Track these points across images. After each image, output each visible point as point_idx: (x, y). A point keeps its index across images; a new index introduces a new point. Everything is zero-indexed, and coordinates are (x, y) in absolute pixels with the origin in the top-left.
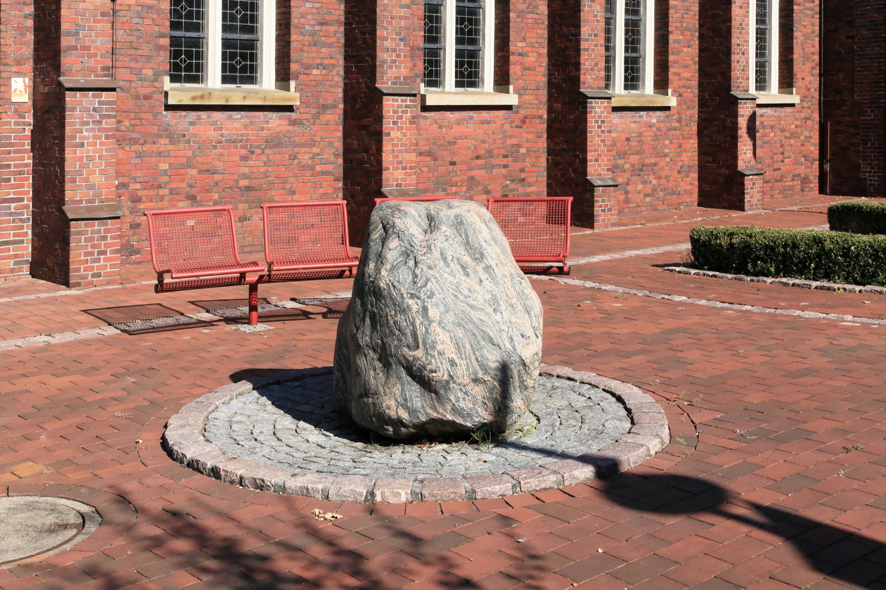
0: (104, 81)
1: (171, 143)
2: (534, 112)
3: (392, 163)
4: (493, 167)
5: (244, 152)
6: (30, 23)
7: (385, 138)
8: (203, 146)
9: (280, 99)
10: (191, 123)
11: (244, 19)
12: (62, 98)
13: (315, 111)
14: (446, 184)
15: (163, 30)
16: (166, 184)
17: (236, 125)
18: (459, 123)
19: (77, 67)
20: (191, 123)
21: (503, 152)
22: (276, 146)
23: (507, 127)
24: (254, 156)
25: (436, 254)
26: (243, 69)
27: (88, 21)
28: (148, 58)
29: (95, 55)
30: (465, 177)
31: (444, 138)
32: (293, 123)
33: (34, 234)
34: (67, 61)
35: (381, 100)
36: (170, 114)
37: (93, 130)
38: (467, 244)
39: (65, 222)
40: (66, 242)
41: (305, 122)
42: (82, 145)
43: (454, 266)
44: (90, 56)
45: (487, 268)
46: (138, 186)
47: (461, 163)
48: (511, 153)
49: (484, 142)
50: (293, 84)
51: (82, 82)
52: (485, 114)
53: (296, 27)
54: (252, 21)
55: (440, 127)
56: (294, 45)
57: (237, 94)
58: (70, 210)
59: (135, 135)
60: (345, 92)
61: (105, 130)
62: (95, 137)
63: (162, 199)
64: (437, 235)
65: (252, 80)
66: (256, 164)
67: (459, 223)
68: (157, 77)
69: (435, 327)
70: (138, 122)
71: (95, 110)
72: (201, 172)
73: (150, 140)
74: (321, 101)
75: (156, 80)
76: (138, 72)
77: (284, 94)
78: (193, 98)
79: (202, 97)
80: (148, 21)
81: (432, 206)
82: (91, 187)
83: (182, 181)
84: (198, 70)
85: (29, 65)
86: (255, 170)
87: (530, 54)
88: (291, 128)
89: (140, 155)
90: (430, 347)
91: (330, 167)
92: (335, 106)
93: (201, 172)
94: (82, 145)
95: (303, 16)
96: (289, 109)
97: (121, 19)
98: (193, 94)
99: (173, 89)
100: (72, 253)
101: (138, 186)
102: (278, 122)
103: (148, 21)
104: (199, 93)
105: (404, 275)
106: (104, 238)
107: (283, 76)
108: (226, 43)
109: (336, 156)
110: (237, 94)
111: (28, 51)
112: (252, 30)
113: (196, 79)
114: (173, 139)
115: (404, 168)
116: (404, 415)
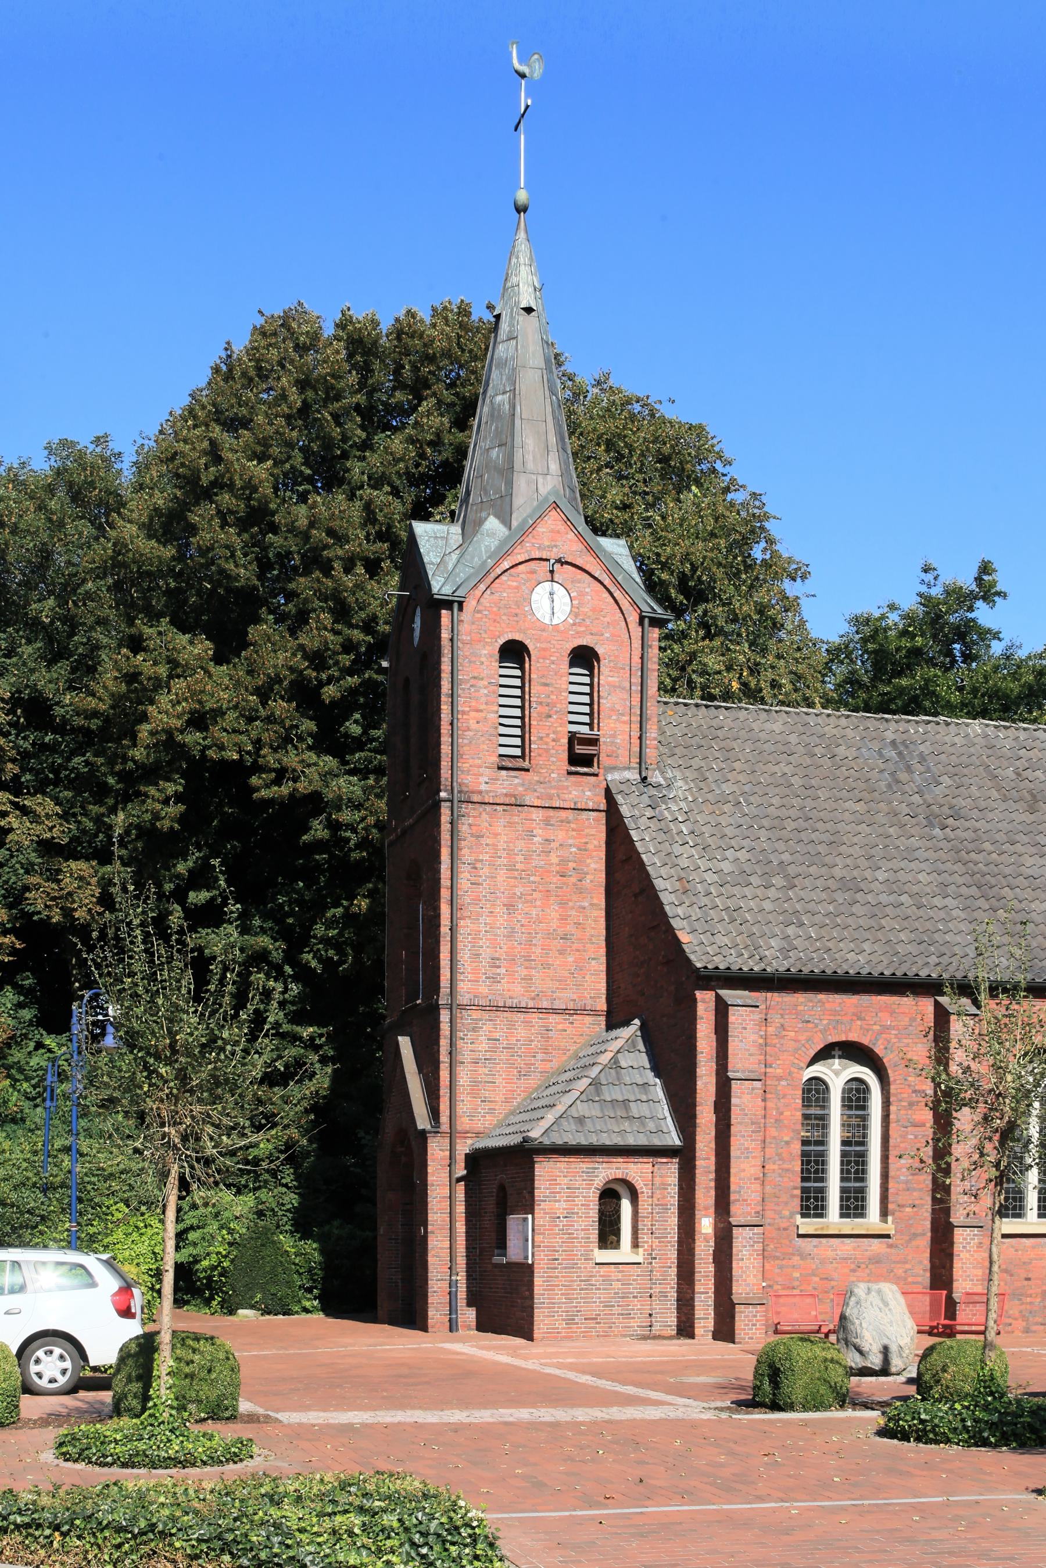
0: (755, 1220)
1: (802, 1259)
3: (961, 1276)
5: (853, 1266)
6: (712, 1184)
7: (955, 1258)
8: (823, 1262)
11: (857, 1172)
12: (731, 1232)
13: (908, 1238)
18: (1033, 1248)
19: (739, 1212)
20: (815, 1246)
22: (877, 1262)
25: (869, 1303)
26: (856, 1208)
28: (786, 1203)
30: (1040, 1290)
32: (890, 1246)
33: (715, 1314)
34: (734, 1209)
35: (953, 1231)
36: (801, 1239)
38: (882, 1300)
39: (733, 1305)
40: (733, 1317)
43: (876, 1308)
45: (890, 1310)
50: (890, 1218)
51: (742, 1221)
53: (893, 1178)
54: (863, 1173)
55: (1016, 1250)
56: (891, 1191)
57: (850, 1225)
58: (735, 1298)
59: (777, 1254)
60: (932, 1223)
64: (871, 1296)
65: (862, 1215)
67: (879, 1292)
68: (792, 1215)
69: (864, 1331)
72: (821, 1279)
74: (913, 1231)
76: (779, 1213)
77: (884, 1225)
78: (816, 1230)
79: (822, 1229)
80: (786, 1179)
81: (870, 1285)
82: (748, 1285)
85: (712, 1210)
88: (888, 1250)
89: (781, 1267)
90: (862, 1338)
91: (920, 1279)
92: (924, 1235)
93: (821, 1279)
95: (899, 1169)
96: (888, 1236)
97: (768, 1178)
99: (802, 1223)
100: (737, 1324)
101: (779, 1287)
103: (786, 1179)
105: (855, 1311)
106: (755, 1316)
107: (884, 1213)
108: (843, 1190)
109: (924, 1270)
110: (850, 1225)
111: (711, 1201)
112: (862, 1180)
113: (821, 1216)
114: (803, 1256)
115: (972, 1280)
116: (853, 1365)
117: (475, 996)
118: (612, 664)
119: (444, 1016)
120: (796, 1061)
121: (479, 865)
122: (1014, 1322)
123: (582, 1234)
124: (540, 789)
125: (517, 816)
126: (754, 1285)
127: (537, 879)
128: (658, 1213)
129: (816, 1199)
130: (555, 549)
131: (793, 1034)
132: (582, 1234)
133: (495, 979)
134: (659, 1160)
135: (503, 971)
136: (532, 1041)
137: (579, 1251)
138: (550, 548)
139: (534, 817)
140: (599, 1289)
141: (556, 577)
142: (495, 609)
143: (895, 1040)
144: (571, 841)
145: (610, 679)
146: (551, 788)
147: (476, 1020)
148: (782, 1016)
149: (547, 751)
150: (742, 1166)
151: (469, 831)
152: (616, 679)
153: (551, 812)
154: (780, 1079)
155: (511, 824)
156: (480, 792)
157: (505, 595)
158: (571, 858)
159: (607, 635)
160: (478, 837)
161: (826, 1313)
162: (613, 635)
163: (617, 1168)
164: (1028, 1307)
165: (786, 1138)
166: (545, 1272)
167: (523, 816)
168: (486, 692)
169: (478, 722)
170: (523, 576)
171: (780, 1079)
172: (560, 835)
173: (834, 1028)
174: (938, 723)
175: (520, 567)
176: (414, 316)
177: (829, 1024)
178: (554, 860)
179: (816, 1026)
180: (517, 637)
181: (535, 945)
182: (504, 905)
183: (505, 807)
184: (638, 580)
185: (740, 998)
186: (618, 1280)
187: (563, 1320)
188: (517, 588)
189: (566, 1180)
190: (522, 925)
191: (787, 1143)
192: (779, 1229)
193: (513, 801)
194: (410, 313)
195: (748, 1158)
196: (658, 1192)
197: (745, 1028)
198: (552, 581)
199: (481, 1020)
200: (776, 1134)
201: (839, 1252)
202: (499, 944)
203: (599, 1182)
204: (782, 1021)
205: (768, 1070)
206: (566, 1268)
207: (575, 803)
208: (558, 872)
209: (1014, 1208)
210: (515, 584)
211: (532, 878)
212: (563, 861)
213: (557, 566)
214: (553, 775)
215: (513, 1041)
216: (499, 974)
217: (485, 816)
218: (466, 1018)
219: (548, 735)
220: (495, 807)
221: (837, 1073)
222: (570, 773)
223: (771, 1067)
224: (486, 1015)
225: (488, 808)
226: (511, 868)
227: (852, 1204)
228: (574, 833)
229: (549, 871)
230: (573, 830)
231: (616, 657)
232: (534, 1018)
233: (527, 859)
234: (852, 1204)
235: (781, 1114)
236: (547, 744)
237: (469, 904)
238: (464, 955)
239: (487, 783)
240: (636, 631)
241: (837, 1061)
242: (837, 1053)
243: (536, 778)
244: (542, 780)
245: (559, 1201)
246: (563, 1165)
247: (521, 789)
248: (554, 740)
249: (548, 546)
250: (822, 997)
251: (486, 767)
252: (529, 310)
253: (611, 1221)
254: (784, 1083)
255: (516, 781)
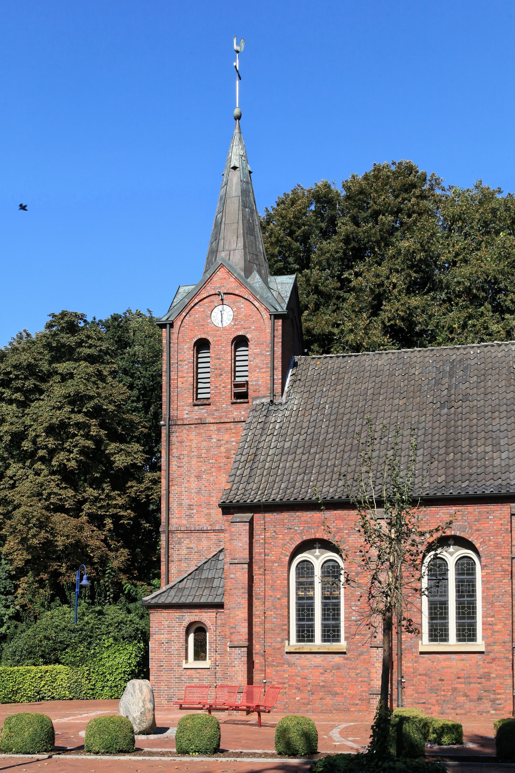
2: (502, 655)
4: (470, 683)
5: (322, 671)
9: (336, 649)
10: (297, 659)
11: (334, 615)
14: (437, 690)
15: (284, 623)
16: (287, 682)
17: (318, 660)
20: (297, 659)
21: (478, 676)
22: (338, 669)
23: (481, 663)
24: (327, 673)
26: (334, 636)
27: (239, 623)
29: (242, 635)
31: (435, 667)
37: (238, 661)
41: (352, 659)
42: (235, 666)
44: (240, 635)
46: (276, 683)
47: (447, 680)
48: (487, 676)
49: (463, 670)
52: (464, 656)
59: (275, 664)
61: (243, 661)
62: (239, 664)
63: (286, 688)
65: (312, 641)
66: (328, 676)
70: (275, 658)
71: (239, 654)
72: (302, 678)
73: (280, 665)
75: (282, 642)
78: (296, 649)
79: (299, 649)
82: (238, 681)
83: (294, 681)
84: (445, 636)
86: (327, 679)
87: (498, 624)
88: (345, 661)
93: (302, 678)
94: (235, 666)
98: (295, 647)
101: (276, 683)
102: (338, 659)
104: (298, 647)
110: (306, 646)
114: (290, 665)
117: (179, 526)
118: (256, 343)
119: (163, 537)
120: (284, 552)
121: (182, 457)
122: (432, 707)
123: (176, 652)
124: (217, 414)
125: (202, 429)
126: (241, 681)
127: (214, 461)
128: (219, 640)
129: (308, 631)
130: (223, 288)
131: (281, 536)
132: (176, 652)
133: (190, 516)
134: (219, 610)
135: (195, 511)
136: (211, 548)
137: (174, 662)
138: (220, 288)
139: (212, 428)
140: (186, 683)
141: (225, 302)
142: (191, 324)
143: (346, 536)
144: (233, 439)
145: (255, 350)
146: (223, 412)
147: (180, 538)
148: (275, 526)
149: (220, 393)
150: (237, 613)
151: (176, 440)
152: (259, 350)
153: (221, 425)
154: (274, 562)
155: (199, 434)
156: (182, 419)
157: (197, 316)
158: (233, 448)
159: (253, 328)
160: (181, 442)
161: (305, 699)
162: (256, 327)
163: (196, 616)
164: (442, 698)
165: (278, 596)
166: (155, 673)
167: (206, 429)
168: (187, 367)
169: (182, 383)
170: (207, 305)
171: (274, 562)
172: (226, 437)
173: (307, 531)
174: (493, 346)
175: (205, 300)
176: (329, 187)
177: (303, 529)
178: (223, 449)
179: (296, 530)
180: (203, 336)
181: (212, 496)
182: (195, 477)
183: (196, 426)
184: (179, 297)
185: (239, 517)
186: (197, 678)
187: (166, 699)
188: (203, 311)
189: (167, 623)
190: (205, 487)
191: (279, 599)
192: (274, 649)
193: (199, 421)
194: (327, 186)
195: (240, 608)
196: (220, 628)
197: (240, 535)
198: (223, 304)
199: (182, 538)
200: (272, 594)
201: (313, 663)
202: (193, 497)
203: (186, 623)
204: (275, 529)
205: (266, 558)
206: (167, 671)
207: (234, 419)
208: (225, 457)
209: (441, 635)
210: (202, 309)
211: (211, 461)
212: (228, 450)
213: (225, 297)
214: (223, 406)
215: (200, 548)
216: (193, 513)
217: (185, 431)
218: (175, 538)
219: (220, 384)
220: (190, 426)
221: (317, 558)
222: (195, 405)
223: (268, 556)
224: (185, 536)
225: (186, 427)
226: (199, 457)
227: (331, 633)
228: (234, 435)
229: (220, 457)
230: (234, 433)
231: (258, 338)
232: (212, 536)
233: (208, 451)
234: (331, 633)
235: (275, 582)
236: (220, 389)
237: (176, 478)
238: (174, 505)
239: (187, 414)
240: (268, 323)
241: (317, 550)
242: (317, 545)
243: (214, 408)
244: (217, 408)
245: (163, 634)
246: (165, 614)
247: (206, 415)
248: (223, 387)
249: (219, 287)
250: (299, 514)
251: (187, 406)
252: (235, 168)
253: (201, 645)
254: (276, 565)
255: (204, 411)
